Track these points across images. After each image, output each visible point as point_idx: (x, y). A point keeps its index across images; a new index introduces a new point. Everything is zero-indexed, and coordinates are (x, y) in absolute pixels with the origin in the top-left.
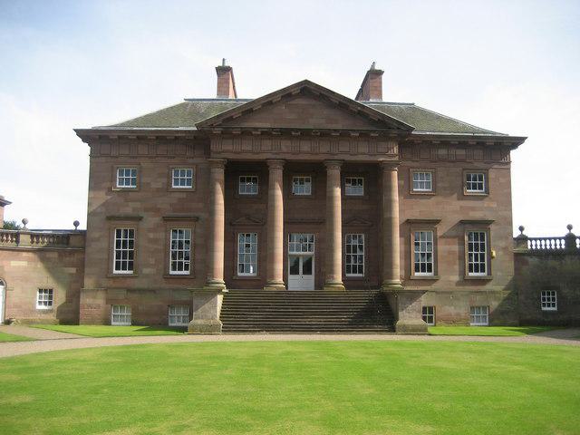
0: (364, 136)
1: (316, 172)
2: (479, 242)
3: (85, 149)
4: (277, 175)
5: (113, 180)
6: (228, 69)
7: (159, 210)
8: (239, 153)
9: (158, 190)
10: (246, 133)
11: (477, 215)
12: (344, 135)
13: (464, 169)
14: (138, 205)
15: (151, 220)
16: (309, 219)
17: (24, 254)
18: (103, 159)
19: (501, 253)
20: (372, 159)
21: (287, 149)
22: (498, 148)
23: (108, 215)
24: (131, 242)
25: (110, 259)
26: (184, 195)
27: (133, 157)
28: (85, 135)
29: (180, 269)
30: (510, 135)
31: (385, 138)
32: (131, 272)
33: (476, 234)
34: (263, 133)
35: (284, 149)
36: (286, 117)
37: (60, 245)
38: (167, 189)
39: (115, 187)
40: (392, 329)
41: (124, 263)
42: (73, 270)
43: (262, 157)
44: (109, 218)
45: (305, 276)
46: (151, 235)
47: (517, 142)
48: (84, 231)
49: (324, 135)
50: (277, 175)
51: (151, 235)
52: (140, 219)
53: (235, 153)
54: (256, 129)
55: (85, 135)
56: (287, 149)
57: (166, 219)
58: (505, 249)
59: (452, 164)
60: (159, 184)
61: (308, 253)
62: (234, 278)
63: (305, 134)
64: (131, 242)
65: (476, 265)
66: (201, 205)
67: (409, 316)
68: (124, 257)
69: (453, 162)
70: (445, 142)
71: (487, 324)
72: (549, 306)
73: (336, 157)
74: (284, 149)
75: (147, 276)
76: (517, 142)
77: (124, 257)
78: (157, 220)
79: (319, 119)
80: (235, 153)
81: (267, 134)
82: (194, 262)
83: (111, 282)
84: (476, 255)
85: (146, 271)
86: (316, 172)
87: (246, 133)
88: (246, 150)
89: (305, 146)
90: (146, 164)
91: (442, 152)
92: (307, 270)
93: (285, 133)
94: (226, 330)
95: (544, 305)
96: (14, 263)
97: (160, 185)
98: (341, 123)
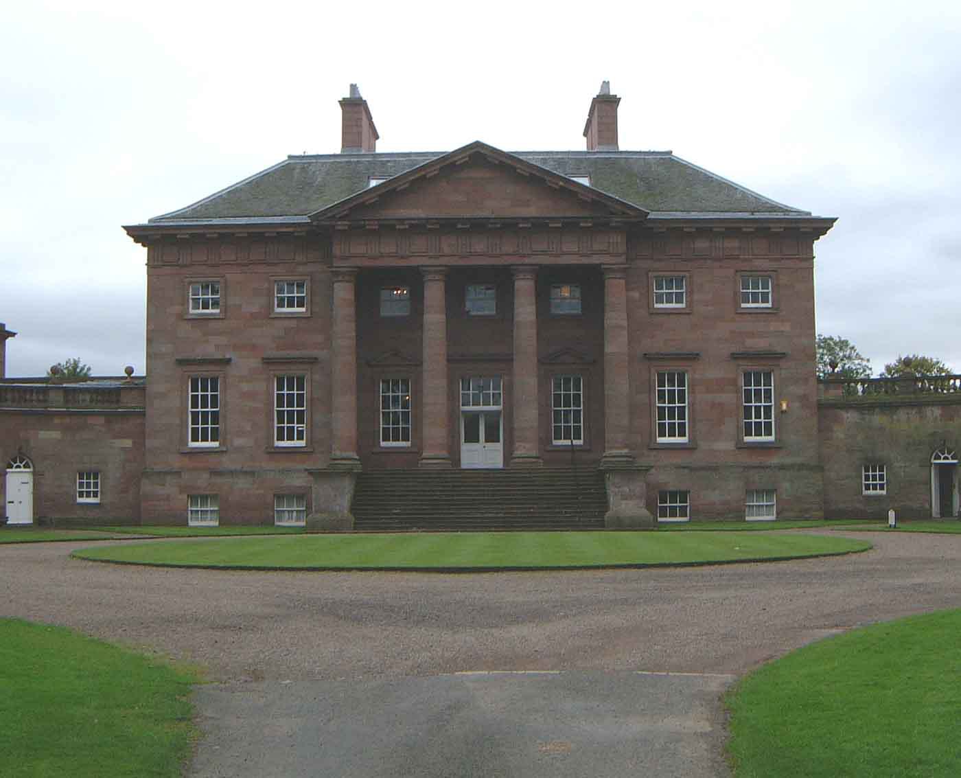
0: (570, 226)
1: (500, 280)
2: (200, 393)
3: (140, 253)
4: (524, 286)
5: (184, 302)
6: (615, 101)
7: (254, 347)
8: (374, 258)
9: (254, 316)
10: (388, 229)
11: (760, 344)
12: (539, 226)
13: (737, 271)
14: (223, 340)
15: (244, 364)
16: (480, 354)
17: (57, 421)
18: (167, 270)
19: (797, 404)
20: (585, 261)
21: (451, 252)
22: (799, 233)
23: (179, 357)
24: (214, 398)
25: (692, 420)
26: (293, 323)
27: (213, 266)
28: (138, 233)
29: (291, 438)
30: (815, 214)
31: (601, 228)
32: (216, 444)
33: (204, 381)
34: (412, 226)
35: (446, 250)
36: (453, 202)
37: (106, 405)
38: (267, 315)
39: (188, 313)
40: (601, 525)
41: (205, 430)
42: (128, 443)
43: (414, 262)
44: (181, 362)
45: (489, 445)
46: (245, 387)
47: (822, 226)
48: (130, 386)
49: (508, 227)
50: (524, 286)
51: (245, 387)
52: (228, 361)
53: (370, 258)
54: (402, 221)
55: (138, 233)
56: (451, 252)
57: (268, 362)
58: (803, 398)
59: (717, 264)
60: (254, 306)
61: (492, 408)
62: (375, 450)
63: (478, 226)
64: (214, 398)
65: (758, 424)
66: (320, 338)
67: (624, 500)
68: (205, 422)
69: (719, 260)
70: (733, 230)
71: (773, 517)
72: (875, 488)
73: (527, 261)
74: (446, 250)
75: (240, 450)
76: (822, 226)
77: (205, 422)
78: (254, 363)
79: (500, 202)
80: (370, 258)
81: (418, 228)
82: (312, 426)
83: (186, 460)
84: (758, 409)
85: (238, 442)
86: (500, 280)
87: (388, 229)
88: (386, 253)
89: (480, 245)
90: (233, 276)
91: (702, 244)
92: (492, 437)
93: (448, 226)
94: (358, 527)
95: (867, 487)
96: (44, 435)
97: (255, 309)
98: (535, 207)
